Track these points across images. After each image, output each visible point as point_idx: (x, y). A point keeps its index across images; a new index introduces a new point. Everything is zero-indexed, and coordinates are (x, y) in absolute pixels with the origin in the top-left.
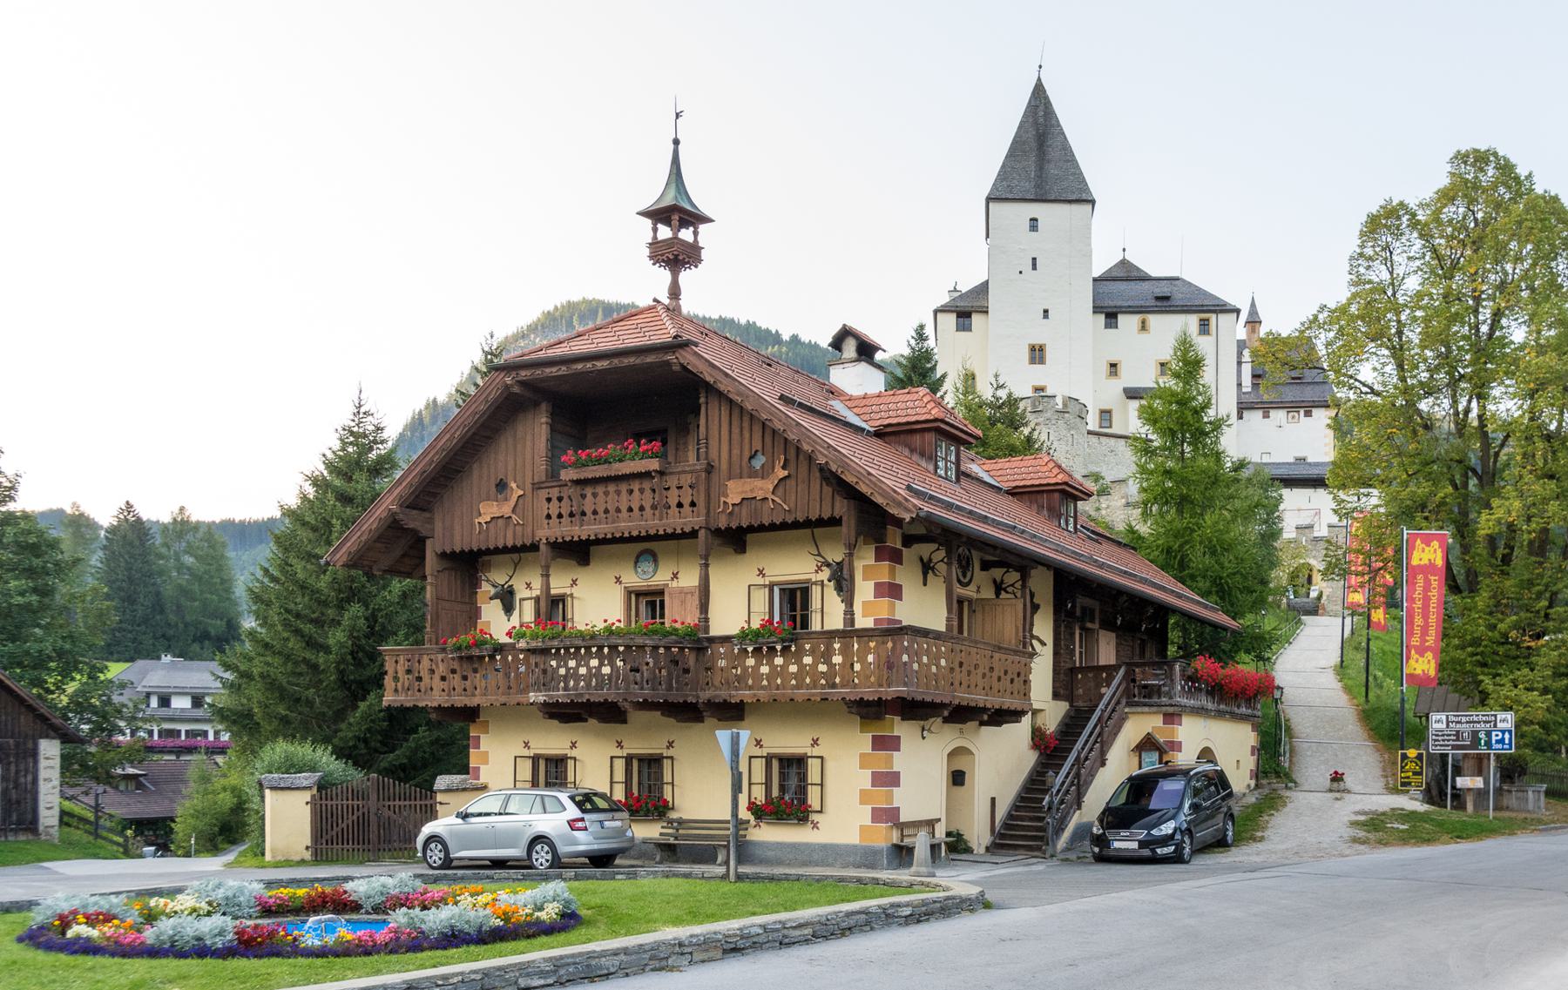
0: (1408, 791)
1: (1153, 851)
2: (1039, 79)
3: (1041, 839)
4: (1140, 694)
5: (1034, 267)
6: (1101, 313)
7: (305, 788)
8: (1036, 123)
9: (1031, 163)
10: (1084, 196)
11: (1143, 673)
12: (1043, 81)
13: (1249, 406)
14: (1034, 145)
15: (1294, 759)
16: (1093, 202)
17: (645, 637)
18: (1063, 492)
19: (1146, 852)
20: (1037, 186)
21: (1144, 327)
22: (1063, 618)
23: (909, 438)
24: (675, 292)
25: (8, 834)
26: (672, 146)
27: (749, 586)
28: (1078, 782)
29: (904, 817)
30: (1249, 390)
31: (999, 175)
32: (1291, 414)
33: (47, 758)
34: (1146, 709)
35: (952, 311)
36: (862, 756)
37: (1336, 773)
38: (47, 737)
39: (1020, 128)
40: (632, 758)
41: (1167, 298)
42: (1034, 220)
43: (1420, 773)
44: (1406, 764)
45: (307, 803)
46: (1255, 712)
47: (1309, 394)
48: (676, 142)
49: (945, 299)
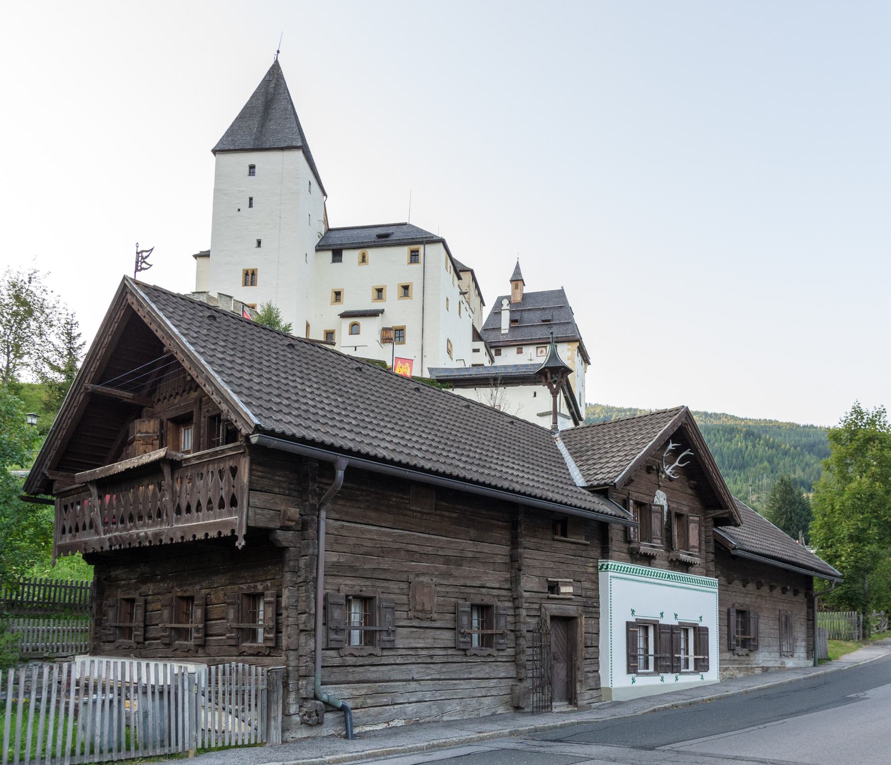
2: (276, 62)
5: (251, 205)
6: (329, 250)
8: (267, 93)
9: (255, 123)
13: (505, 344)
14: (261, 108)
20: (256, 139)
21: (364, 259)
25: (826, 620)
30: (507, 331)
31: (227, 132)
32: (539, 350)
39: (252, 97)
41: (386, 236)
42: (252, 167)
47: (558, 332)
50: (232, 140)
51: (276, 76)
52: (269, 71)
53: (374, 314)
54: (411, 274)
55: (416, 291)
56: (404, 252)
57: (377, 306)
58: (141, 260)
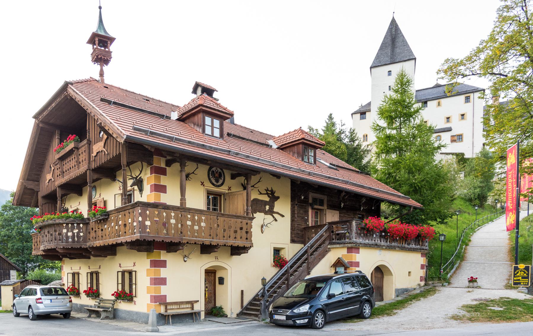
0: (517, 288)
1: (294, 321)
2: (393, 17)
3: (258, 310)
4: (336, 238)
7: (10, 285)
8: (391, 35)
9: (389, 51)
10: (411, 58)
11: (337, 227)
12: (395, 18)
14: (390, 43)
15: (457, 271)
16: (415, 59)
17: (59, 219)
18: (303, 143)
19: (291, 322)
20: (391, 58)
21: (439, 104)
22: (296, 203)
23: (192, 119)
24: (102, 74)
26: (99, 10)
27: (115, 195)
28: (288, 283)
29: (168, 300)
31: (375, 58)
33: (13, 276)
34: (338, 246)
35: (358, 113)
36: (147, 270)
37: (472, 277)
38: (12, 270)
40: (75, 274)
42: (390, 71)
43: (527, 278)
44: (518, 273)
45: (12, 290)
46: (424, 247)
48: (100, 8)
49: (356, 108)
50: (379, 61)
51: (395, 25)
52: (391, 23)
53: (449, 130)
54: (466, 108)
55: (468, 116)
56: (463, 97)
57: (448, 125)
58: (301, 127)
